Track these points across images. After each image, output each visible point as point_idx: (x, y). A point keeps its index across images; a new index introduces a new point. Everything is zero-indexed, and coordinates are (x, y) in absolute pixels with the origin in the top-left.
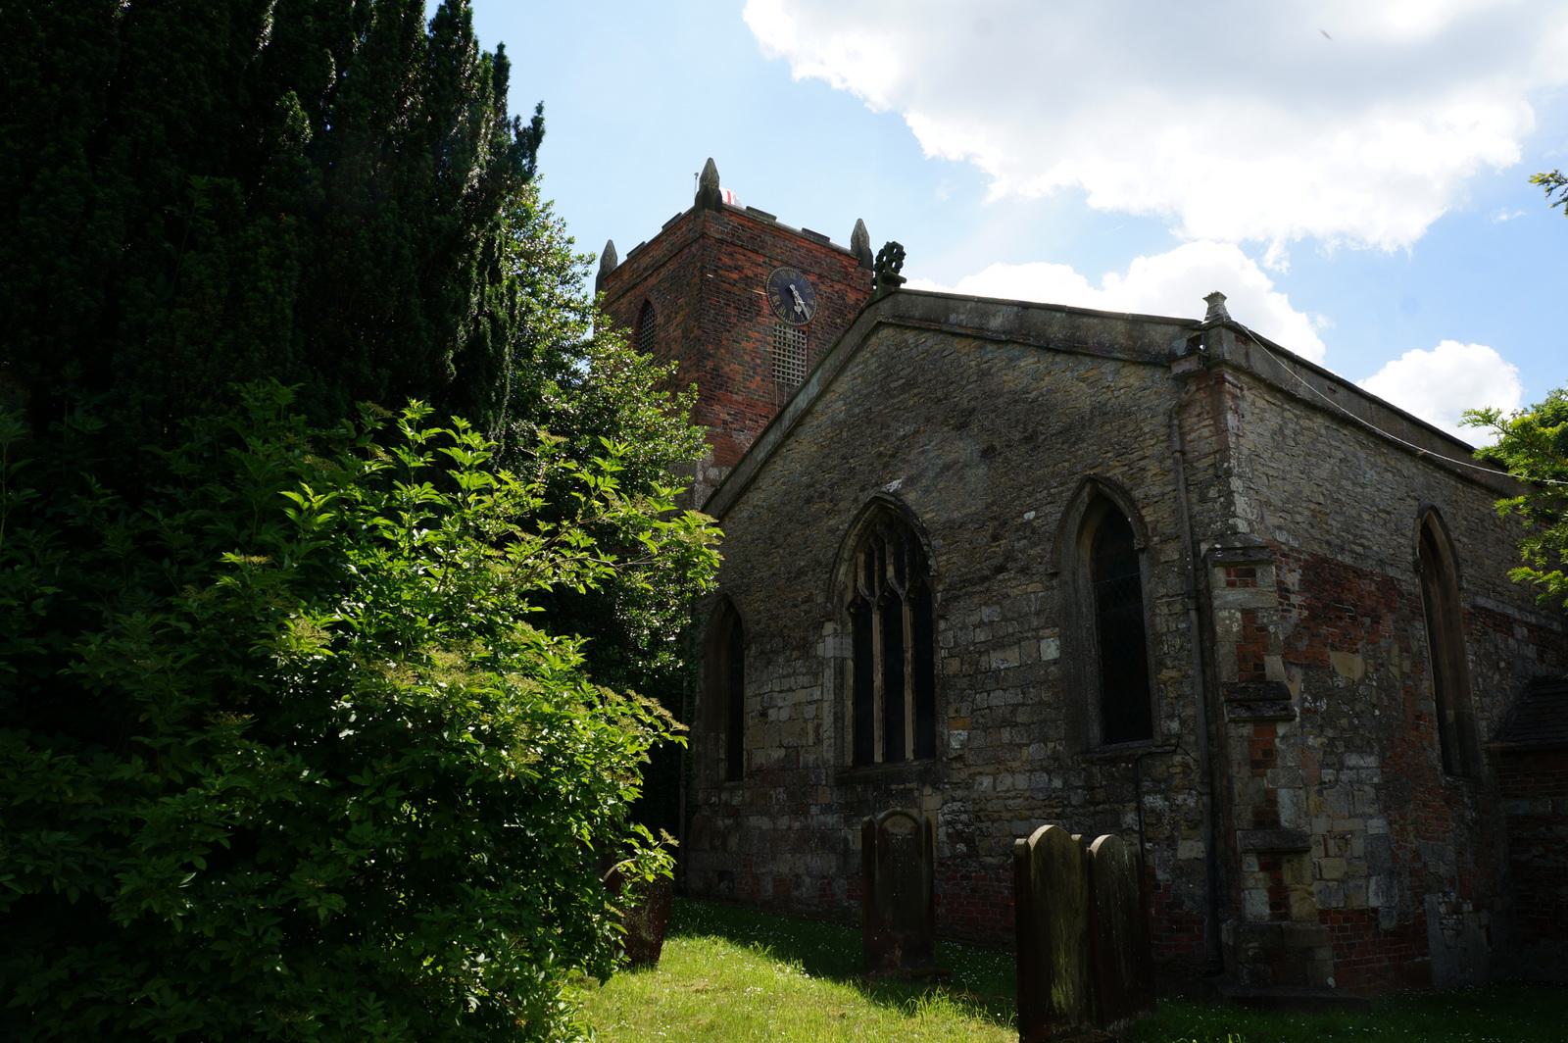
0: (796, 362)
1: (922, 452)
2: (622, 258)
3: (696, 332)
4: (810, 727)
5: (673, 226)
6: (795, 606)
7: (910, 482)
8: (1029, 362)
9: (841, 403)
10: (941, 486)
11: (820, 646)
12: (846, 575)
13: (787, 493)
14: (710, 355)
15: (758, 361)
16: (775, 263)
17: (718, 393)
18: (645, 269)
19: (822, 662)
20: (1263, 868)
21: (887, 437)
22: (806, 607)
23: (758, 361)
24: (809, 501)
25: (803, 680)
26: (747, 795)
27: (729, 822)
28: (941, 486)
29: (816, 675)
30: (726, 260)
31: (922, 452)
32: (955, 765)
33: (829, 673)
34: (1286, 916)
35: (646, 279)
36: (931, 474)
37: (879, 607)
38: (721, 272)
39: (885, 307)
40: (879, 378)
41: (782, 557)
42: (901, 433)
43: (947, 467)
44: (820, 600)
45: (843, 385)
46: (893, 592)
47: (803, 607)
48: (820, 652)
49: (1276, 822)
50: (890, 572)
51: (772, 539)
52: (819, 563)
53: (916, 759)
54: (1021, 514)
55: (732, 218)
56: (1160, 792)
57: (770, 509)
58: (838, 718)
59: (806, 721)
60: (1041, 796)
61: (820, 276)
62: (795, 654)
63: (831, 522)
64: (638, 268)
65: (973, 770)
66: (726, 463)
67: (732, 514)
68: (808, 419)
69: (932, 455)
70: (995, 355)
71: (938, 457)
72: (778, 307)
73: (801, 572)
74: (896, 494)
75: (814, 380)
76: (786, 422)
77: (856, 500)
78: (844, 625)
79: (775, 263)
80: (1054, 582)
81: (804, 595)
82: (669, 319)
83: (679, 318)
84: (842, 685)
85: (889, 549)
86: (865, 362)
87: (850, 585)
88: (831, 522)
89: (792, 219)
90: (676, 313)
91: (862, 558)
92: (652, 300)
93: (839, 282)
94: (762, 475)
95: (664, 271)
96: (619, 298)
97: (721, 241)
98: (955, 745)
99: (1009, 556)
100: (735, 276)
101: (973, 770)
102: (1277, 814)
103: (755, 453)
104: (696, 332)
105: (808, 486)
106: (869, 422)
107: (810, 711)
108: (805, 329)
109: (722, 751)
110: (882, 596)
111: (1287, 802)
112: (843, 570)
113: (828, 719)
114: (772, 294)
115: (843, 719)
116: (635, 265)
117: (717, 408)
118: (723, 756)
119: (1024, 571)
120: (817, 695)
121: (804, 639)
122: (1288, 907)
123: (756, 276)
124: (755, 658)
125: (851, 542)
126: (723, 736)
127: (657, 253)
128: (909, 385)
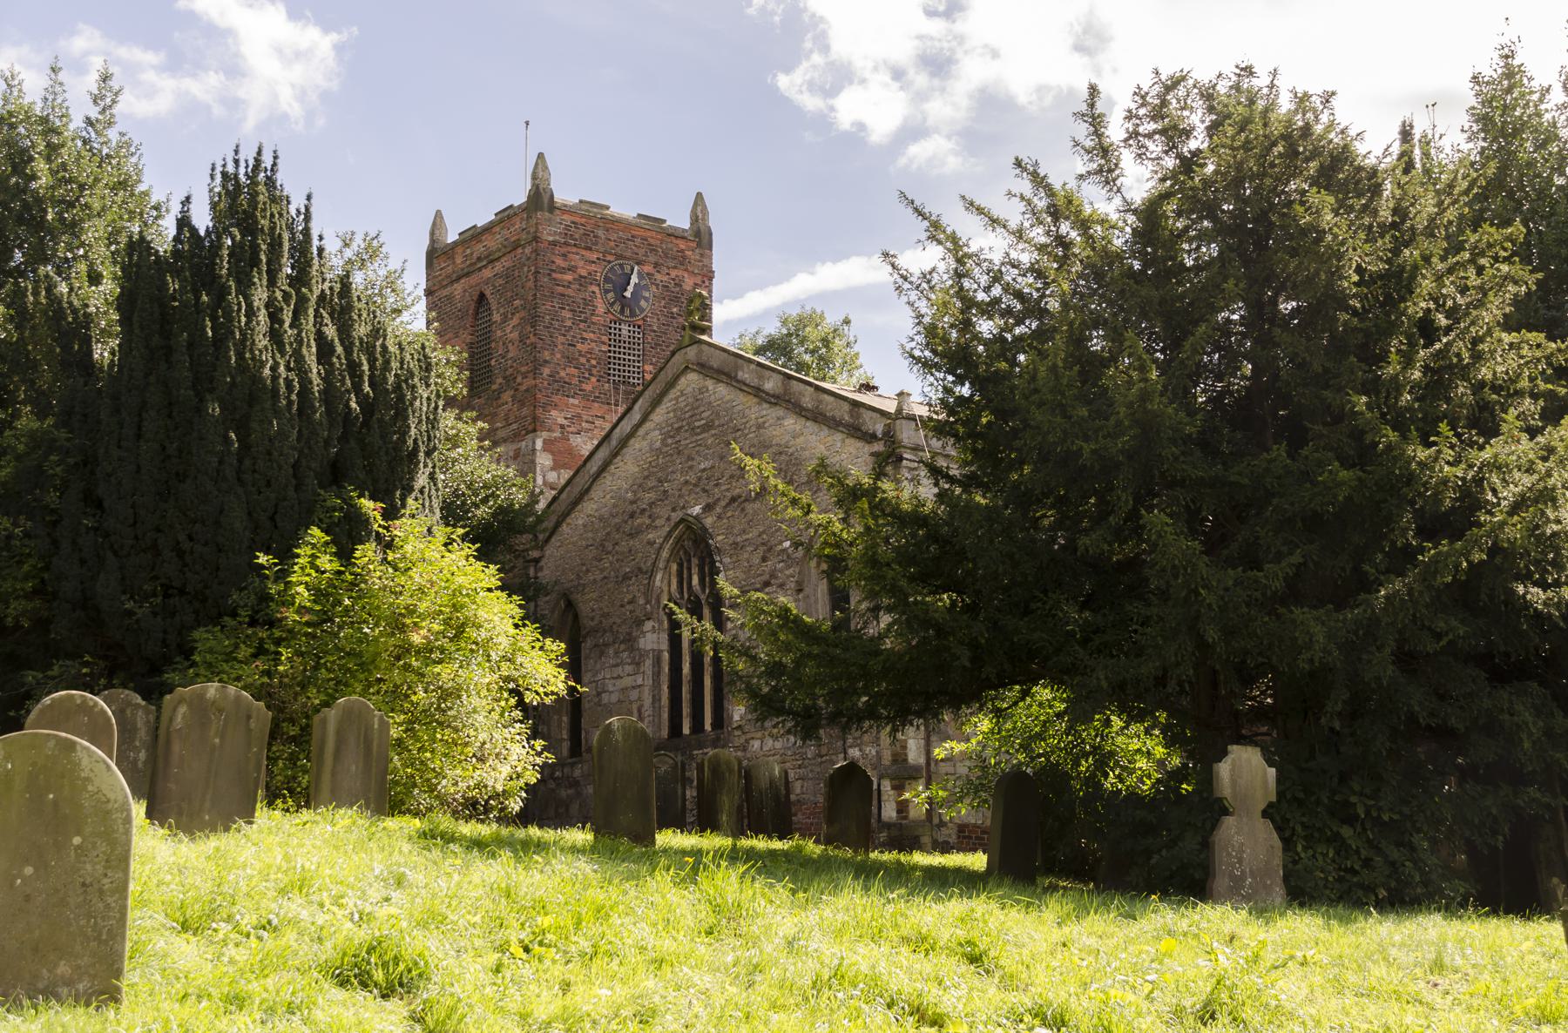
0: (627, 357)
1: (717, 485)
2: (452, 237)
3: (533, 339)
4: (635, 707)
5: (506, 216)
6: (622, 606)
7: (708, 508)
8: (791, 423)
9: (657, 432)
10: (729, 514)
11: (642, 641)
12: (662, 581)
13: (615, 506)
14: (546, 362)
15: (594, 362)
16: (610, 258)
17: (555, 398)
18: (479, 259)
19: (643, 654)
20: (894, 788)
21: (691, 467)
22: (629, 607)
23: (594, 362)
24: (632, 516)
25: (629, 669)
26: (585, 768)
27: (570, 792)
28: (729, 514)
29: (638, 664)
30: (559, 262)
31: (717, 485)
32: (737, 733)
33: (648, 663)
34: (906, 818)
35: (480, 269)
36: (723, 503)
37: (709, 603)
38: (554, 275)
39: (691, 352)
40: (687, 415)
41: (611, 563)
42: (702, 466)
43: (733, 500)
44: (642, 601)
45: (659, 416)
46: (697, 597)
47: (628, 607)
48: (641, 646)
49: (906, 760)
50: (695, 580)
51: (603, 546)
52: (640, 569)
53: (713, 729)
54: (781, 542)
55: (564, 217)
56: (858, 745)
57: (601, 519)
58: (656, 699)
59: (631, 702)
60: (789, 753)
61: (656, 265)
62: (623, 647)
63: (650, 536)
64: (472, 254)
65: (749, 736)
66: (565, 466)
67: (568, 520)
68: (632, 441)
69: (723, 488)
70: (771, 413)
71: (728, 490)
72: (612, 304)
73: (626, 577)
74: (696, 518)
75: (637, 407)
76: (614, 443)
77: (668, 519)
78: (660, 623)
79: (610, 258)
80: (800, 596)
81: (630, 596)
82: (505, 319)
83: (515, 321)
84: (659, 673)
85: (695, 561)
86: (677, 399)
87: (666, 589)
88: (650, 536)
89: (624, 207)
90: (513, 314)
91: (674, 567)
92: (488, 293)
93: (675, 268)
94: (595, 487)
95: (498, 267)
96: (452, 282)
97: (554, 243)
98: (736, 717)
99: (773, 575)
100: (568, 277)
101: (749, 736)
102: (906, 755)
103: (588, 465)
104: (533, 339)
105: (633, 502)
106: (679, 453)
107: (634, 695)
108: (640, 323)
109: (564, 732)
110: (689, 599)
111: (914, 748)
112: (659, 577)
113: (648, 701)
114: (607, 291)
115: (660, 700)
116: (468, 251)
117: (554, 413)
118: (565, 737)
119: (781, 586)
120: (640, 681)
121: (629, 634)
122: (908, 812)
123: (590, 274)
124: (591, 650)
125: (665, 554)
126: (565, 719)
127: (492, 242)
128: (708, 427)
